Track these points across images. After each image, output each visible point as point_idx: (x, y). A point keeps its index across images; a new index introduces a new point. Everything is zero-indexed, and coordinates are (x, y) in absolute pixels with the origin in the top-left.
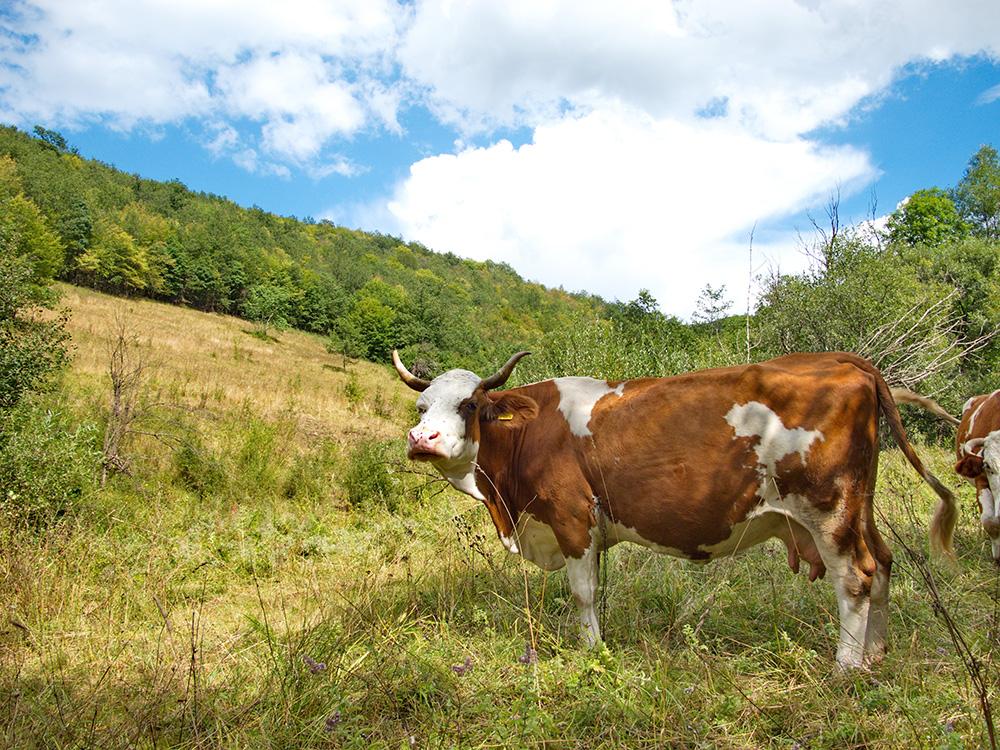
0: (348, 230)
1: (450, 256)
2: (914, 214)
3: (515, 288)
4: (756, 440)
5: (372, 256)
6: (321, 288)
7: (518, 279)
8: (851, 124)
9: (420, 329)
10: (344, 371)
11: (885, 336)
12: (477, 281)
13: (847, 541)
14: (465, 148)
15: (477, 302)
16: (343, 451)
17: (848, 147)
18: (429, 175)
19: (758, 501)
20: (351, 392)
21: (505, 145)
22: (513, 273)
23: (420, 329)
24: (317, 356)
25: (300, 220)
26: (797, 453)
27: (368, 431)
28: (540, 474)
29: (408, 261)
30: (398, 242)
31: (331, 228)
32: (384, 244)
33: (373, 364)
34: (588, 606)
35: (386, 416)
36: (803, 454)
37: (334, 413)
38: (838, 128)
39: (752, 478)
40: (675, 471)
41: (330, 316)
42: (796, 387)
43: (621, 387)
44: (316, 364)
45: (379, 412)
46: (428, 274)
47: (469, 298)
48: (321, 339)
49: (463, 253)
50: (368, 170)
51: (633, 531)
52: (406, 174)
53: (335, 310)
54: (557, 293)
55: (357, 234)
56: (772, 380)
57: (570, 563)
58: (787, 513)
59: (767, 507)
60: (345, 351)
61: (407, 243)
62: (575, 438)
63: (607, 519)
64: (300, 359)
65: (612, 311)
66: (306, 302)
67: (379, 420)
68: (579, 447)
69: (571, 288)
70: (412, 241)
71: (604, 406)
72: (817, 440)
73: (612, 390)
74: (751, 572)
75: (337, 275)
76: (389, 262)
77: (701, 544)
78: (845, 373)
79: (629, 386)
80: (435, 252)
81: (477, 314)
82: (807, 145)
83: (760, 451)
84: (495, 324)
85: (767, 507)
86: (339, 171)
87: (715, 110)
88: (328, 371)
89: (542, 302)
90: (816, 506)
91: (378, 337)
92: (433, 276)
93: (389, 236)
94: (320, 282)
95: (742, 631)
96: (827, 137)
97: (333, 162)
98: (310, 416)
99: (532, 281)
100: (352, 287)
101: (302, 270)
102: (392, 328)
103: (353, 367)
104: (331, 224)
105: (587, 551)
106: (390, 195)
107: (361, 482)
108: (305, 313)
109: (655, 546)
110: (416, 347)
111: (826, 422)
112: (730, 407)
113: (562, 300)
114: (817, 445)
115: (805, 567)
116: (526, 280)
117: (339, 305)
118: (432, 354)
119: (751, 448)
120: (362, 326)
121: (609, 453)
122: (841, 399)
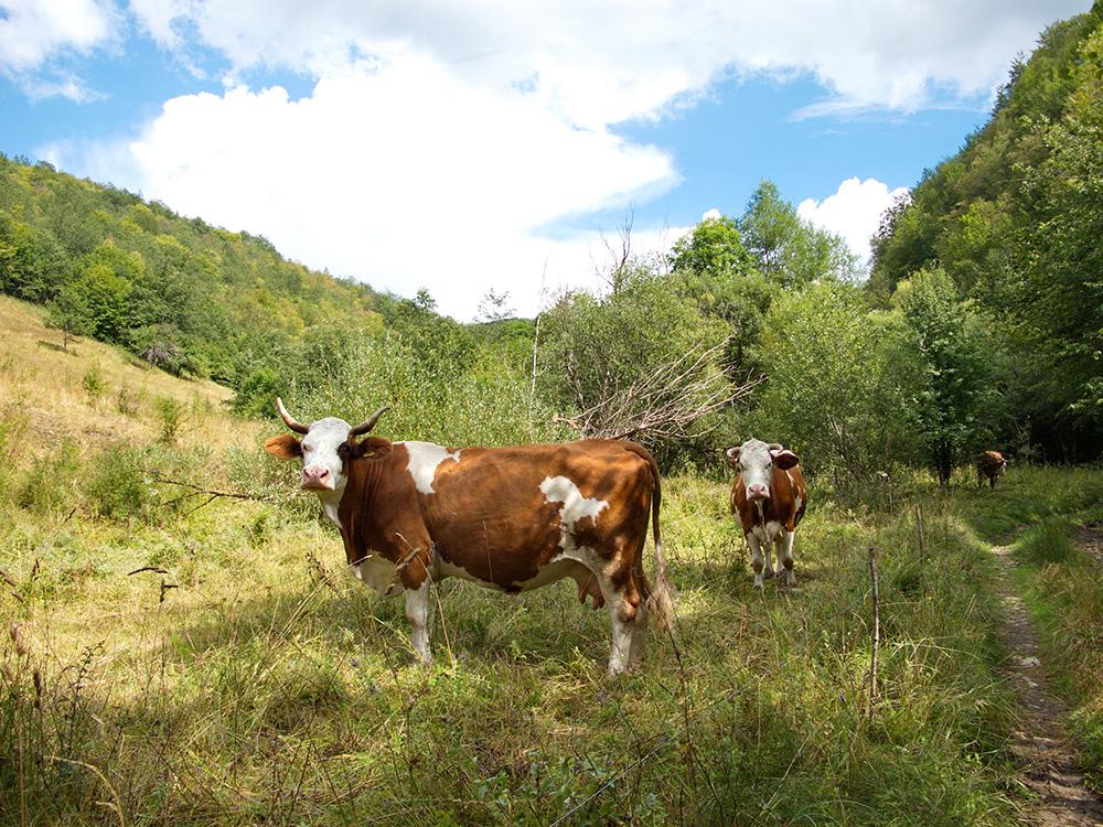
0: (74, 179)
1: (198, 223)
2: (703, 239)
3: (273, 267)
4: (561, 505)
5: (104, 213)
6: (37, 247)
7: (277, 257)
8: (664, 119)
9: (161, 307)
10: (65, 350)
11: (664, 375)
12: (229, 255)
13: (619, 581)
14: (234, 87)
15: (227, 280)
16: (85, 452)
17: (651, 148)
18: (182, 113)
19: (561, 550)
20: (92, 385)
21: (279, 93)
22: (272, 249)
23: (161, 307)
24: (31, 330)
25: (11, 158)
26: (589, 517)
27: (113, 431)
28: (390, 522)
29: (148, 225)
30: (136, 199)
31: (50, 173)
32: (118, 200)
33: (101, 344)
34: (422, 628)
35: (133, 414)
36: (593, 518)
37: (71, 408)
38: (648, 121)
39: (556, 535)
40: (500, 525)
41: (47, 281)
42: (593, 467)
43: (458, 453)
44: (29, 340)
45: (122, 410)
46: (169, 241)
47: (219, 273)
48: (34, 308)
49: (212, 220)
50: (105, 97)
51: (462, 569)
52: (159, 112)
53: (53, 275)
54: (321, 277)
55: (85, 184)
56: (575, 462)
57: (409, 593)
58: (580, 560)
59: (565, 555)
60: (67, 327)
61: (147, 202)
62: (420, 495)
63: (441, 559)
64: (8, 332)
65: (380, 303)
66: (17, 262)
67: (124, 418)
68: (424, 502)
69: (339, 271)
70: (154, 200)
71: (445, 470)
72: (605, 508)
73: (450, 456)
74: (556, 600)
75: (59, 233)
76: (124, 223)
77: (513, 580)
78: (628, 459)
79: (464, 454)
80: (181, 215)
81: (227, 294)
82: (617, 139)
83: (562, 512)
84: (248, 306)
85: (565, 555)
86: (65, 93)
87: (528, 86)
88: (43, 350)
89: (304, 286)
90: (600, 556)
91: (109, 313)
92: (178, 245)
93: (125, 190)
94: (36, 239)
95: (547, 645)
96: (636, 133)
97: (58, 80)
98: (43, 410)
99: (293, 261)
100: (79, 249)
101: (13, 222)
102: (127, 303)
103: (76, 345)
104: (51, 168)
105: (423, 584)
106: (135, 135)
107: (112, 491)
108: (14, 276)
109: (479, 581)
110: (154, 328)
111: (612, 495)
112: (544, 479)
113: (326, 285)
114: (604, 513)
115: (590, 599)
116: (286, 258)
117: (60, 269)
118: (174, 337)
119: (557, 511)
120: (89, 297)
121: (449, 509)
122: (624, 479)
